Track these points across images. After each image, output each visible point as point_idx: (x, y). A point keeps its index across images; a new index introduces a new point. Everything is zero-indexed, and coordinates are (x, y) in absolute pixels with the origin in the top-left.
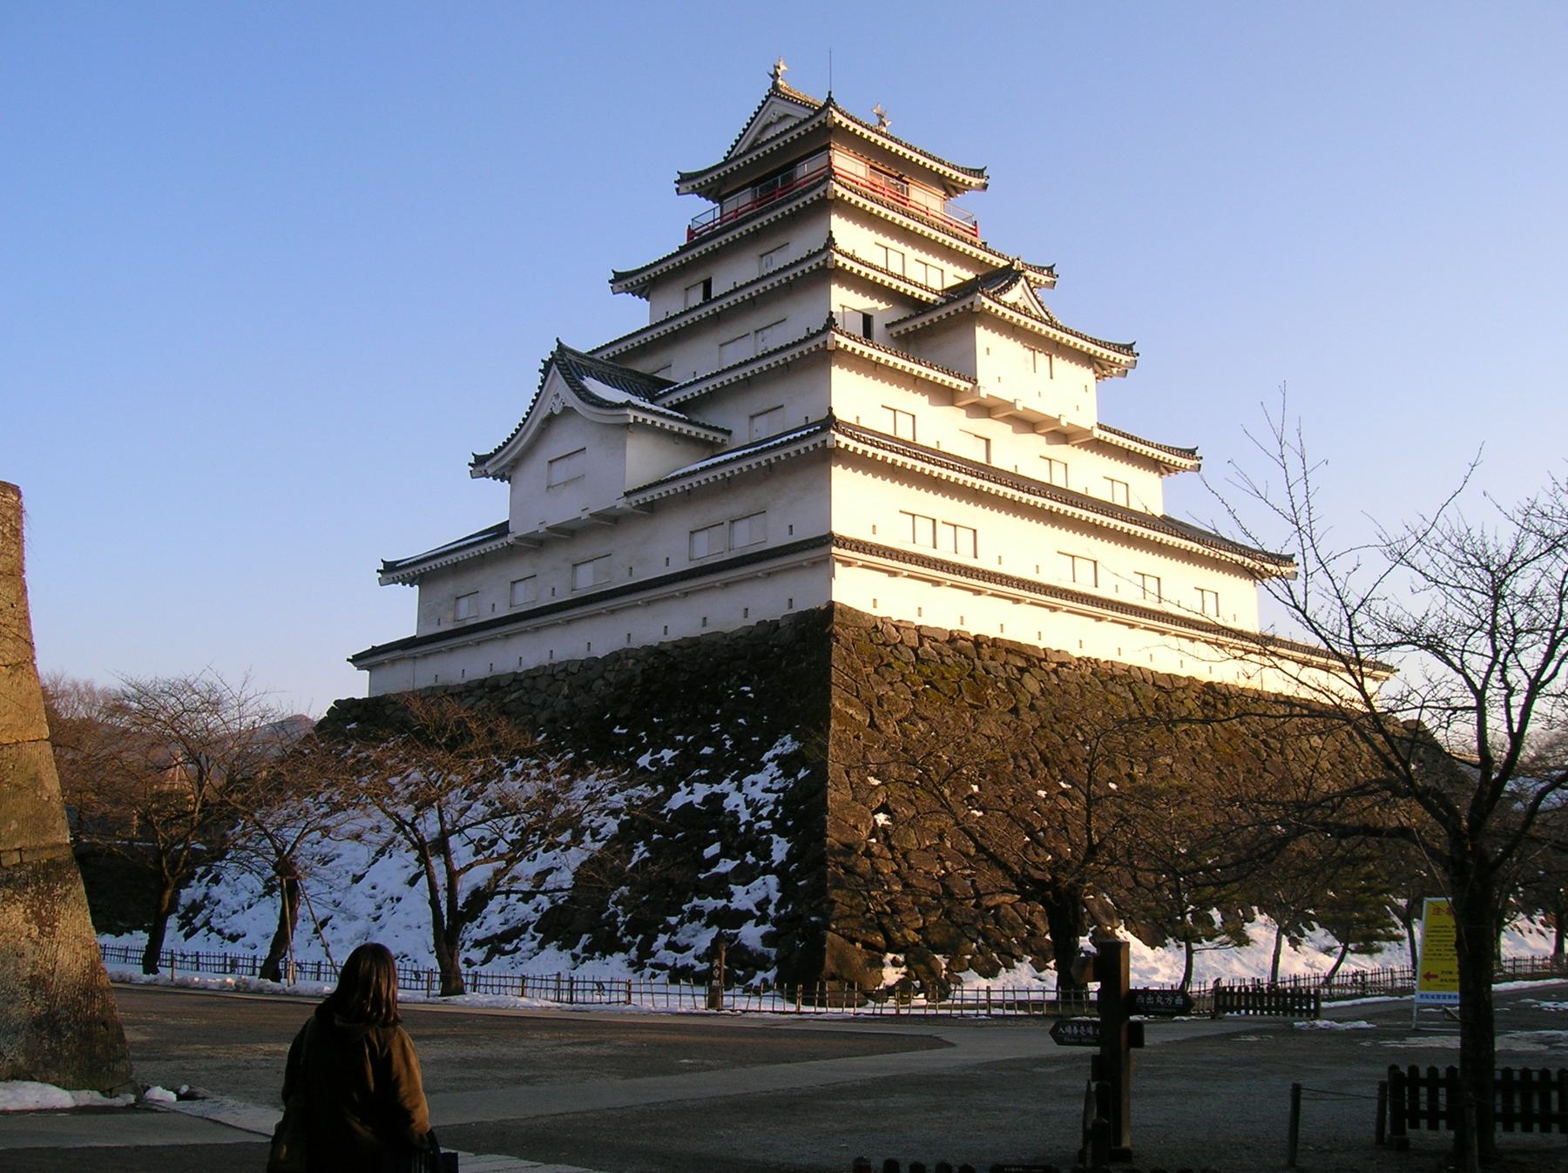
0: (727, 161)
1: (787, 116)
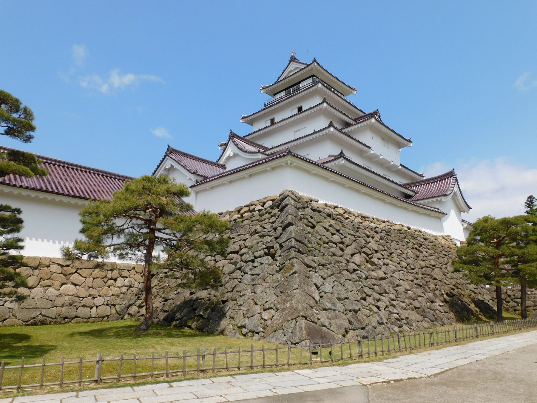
0: (277, 82)
1: (297, 68)
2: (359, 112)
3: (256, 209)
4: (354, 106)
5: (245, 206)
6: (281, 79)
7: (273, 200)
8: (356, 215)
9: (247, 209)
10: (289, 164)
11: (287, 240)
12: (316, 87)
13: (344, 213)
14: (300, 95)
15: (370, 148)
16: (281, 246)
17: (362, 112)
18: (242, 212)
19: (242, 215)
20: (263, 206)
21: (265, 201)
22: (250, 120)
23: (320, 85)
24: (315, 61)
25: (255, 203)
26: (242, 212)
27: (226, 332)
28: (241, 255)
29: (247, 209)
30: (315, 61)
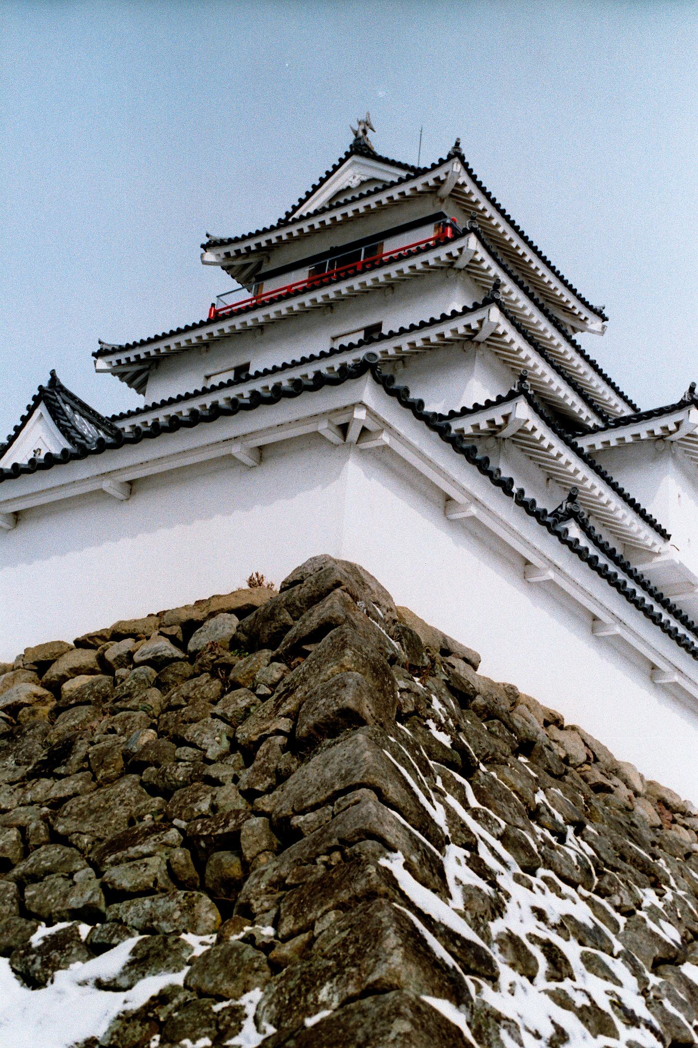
0: (283, 223)
1: (373, 180)
2: (615, 400)
3: (137, 658)
4: (599, 372)
5: (81, 644)
6: (303, 211)
7: (240, 612)
8: (639, 787)
9: (87, 657)
10: (354, 433)
11: (330, 800)
12: (453, 248)
13: (587, 762)
14: (380, 274)
15: (665, 535)
16: (283, 833)
17: (625, 399)
18: (55, 671)
19: (55, 687)
20: (181, 644)
21: (197, 615)
22: (139, 365)
23: (472, 242)
24: (457, 154)
25: (140, 629)
26: (55, 671)
27: (363, 117)
28: (22, 883)
29: (87, 657)
30: (457, 154)
